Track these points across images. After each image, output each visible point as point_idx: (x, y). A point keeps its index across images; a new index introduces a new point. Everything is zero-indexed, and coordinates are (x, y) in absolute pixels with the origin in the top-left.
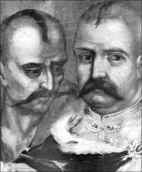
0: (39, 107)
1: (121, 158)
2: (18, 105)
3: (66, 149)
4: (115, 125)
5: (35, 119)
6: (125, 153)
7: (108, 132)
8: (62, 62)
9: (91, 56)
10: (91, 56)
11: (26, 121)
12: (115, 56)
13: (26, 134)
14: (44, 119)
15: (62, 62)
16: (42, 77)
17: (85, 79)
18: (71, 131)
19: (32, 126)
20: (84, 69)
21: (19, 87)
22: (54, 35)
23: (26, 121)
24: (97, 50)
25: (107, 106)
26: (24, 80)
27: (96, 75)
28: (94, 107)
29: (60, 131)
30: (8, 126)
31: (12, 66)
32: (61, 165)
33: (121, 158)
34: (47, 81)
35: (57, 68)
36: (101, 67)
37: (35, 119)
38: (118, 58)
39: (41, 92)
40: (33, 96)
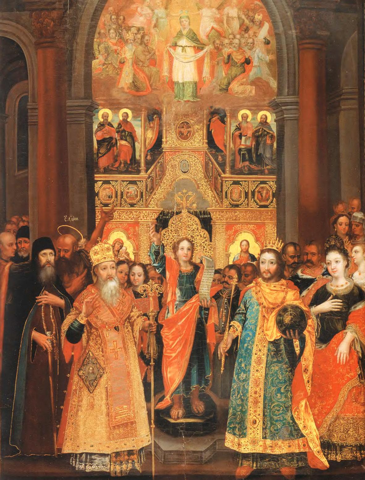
0: (294, 266)
1: (77, 331)
2: (288, 266)
3: (301, 277)
4: (188, 457)
5: (293, 269)
6: (316, 279)
7: (207, 453)
8: (300, 255)
9: (307, 254)
10: (307, 254)
11: (290, 270)
12: (313, 254)
13: (291, 273)
14: (296, 269)
15: (300, 255)
16: (295, 259)
17: (305, 260)
18: (302, 272)
19: (292, 271)
20: (305, 257)
21: (289, 261)
22: (298, 248)
23: (290, 270)
24: (309, 253)
25: (311, 267)
26: (290, 259)
27: (308, 259)
28: (308, 267)
29: (299, 273)
30: (286, 271)
31: (287, 256)
32: (299, 281)
33: (77, 331)
34: (296, 260)
35: (299, 257)
36: (310, 257)
37: (293, 269)
38: (314, 254)
39: (294, 263)
40: (293, 263)
